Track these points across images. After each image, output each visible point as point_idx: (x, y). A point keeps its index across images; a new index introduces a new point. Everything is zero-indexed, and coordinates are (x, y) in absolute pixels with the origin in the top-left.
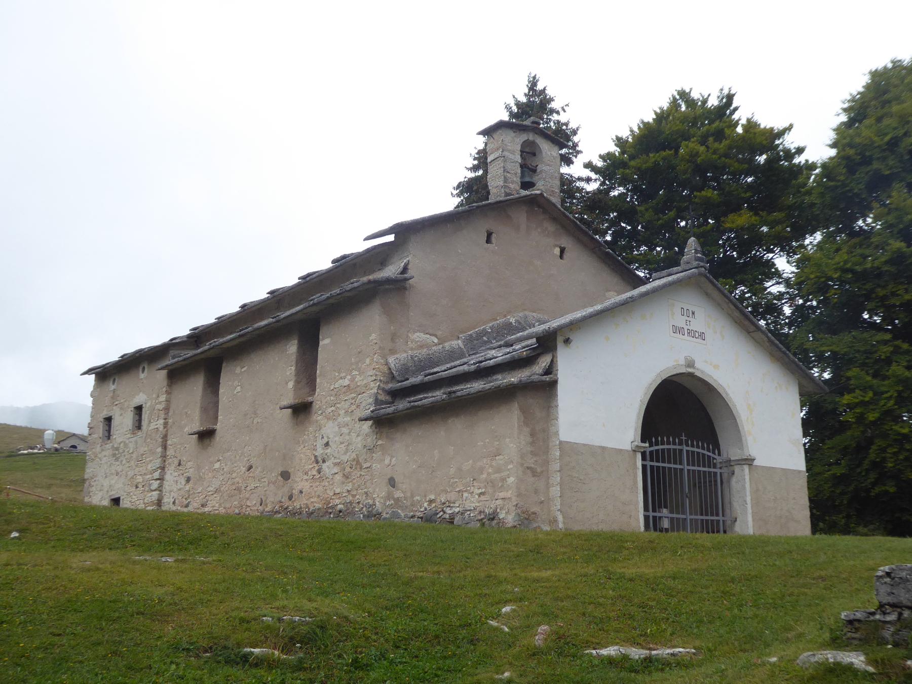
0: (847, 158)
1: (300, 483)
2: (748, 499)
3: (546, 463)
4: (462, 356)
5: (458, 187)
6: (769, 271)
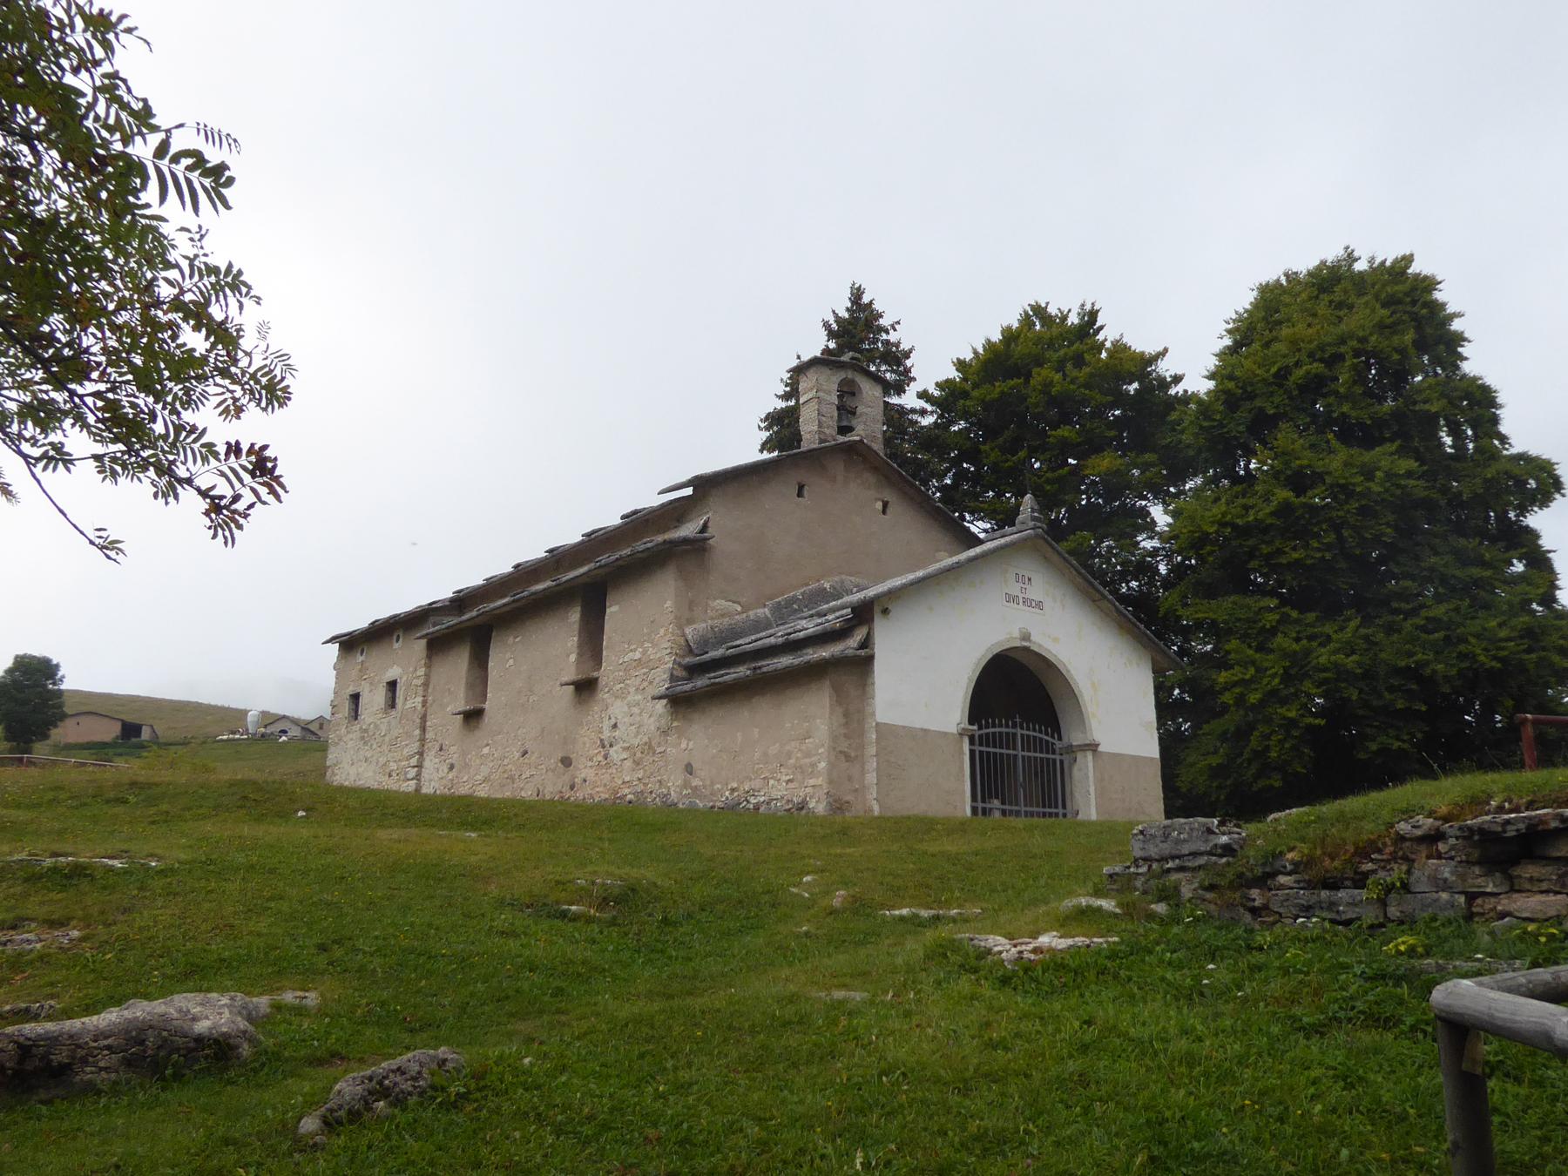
0: (1226, 392)
1: (584, 770)
2: (1092, 789)
3: (862, 747)
4: (768, 626)
5: (766, 419)
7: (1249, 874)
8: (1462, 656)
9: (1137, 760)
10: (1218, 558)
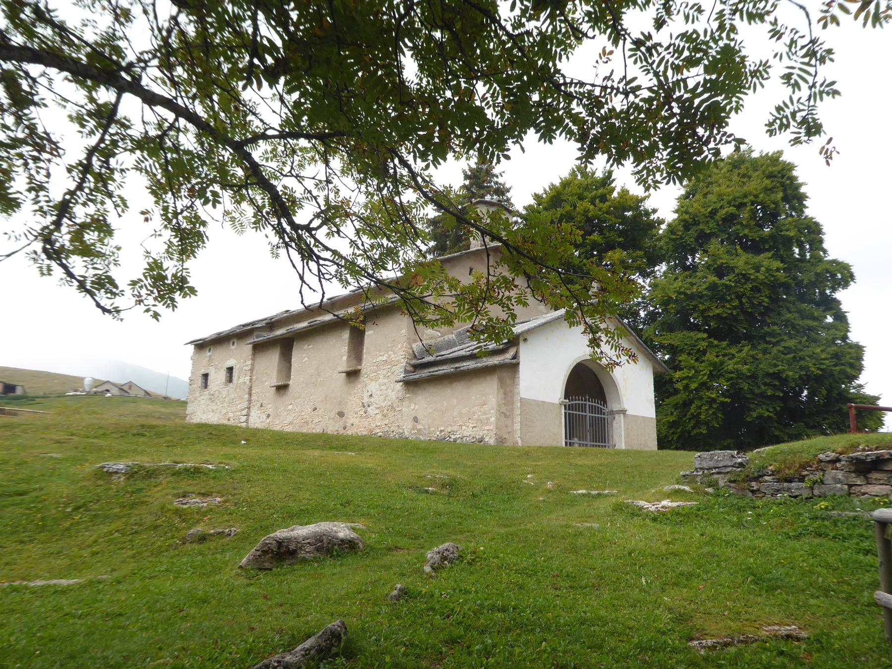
0: (684, 220)
2: (623, 433)
3: (512, 410)
4: (454, 345)
6: (634, 289)
7: (751, 475)
8: (801, 368)
9: (644, 418)
10: (677, 313)
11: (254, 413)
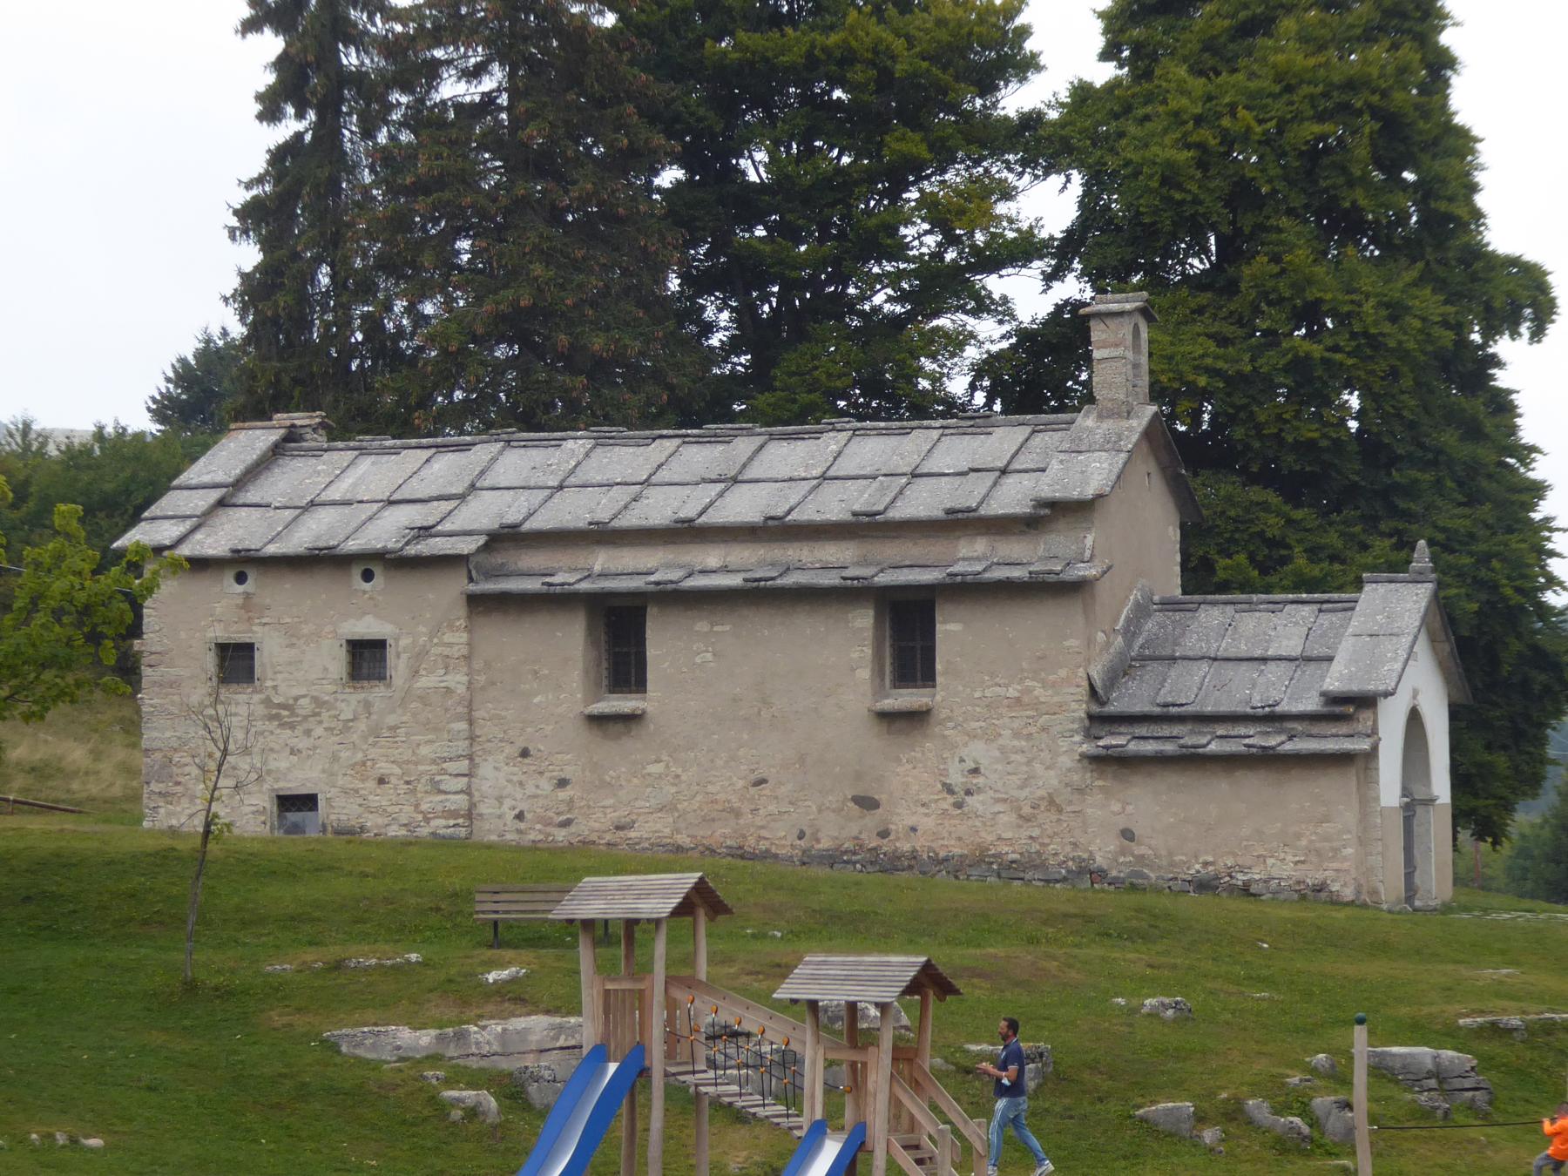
11: (494, 774)
